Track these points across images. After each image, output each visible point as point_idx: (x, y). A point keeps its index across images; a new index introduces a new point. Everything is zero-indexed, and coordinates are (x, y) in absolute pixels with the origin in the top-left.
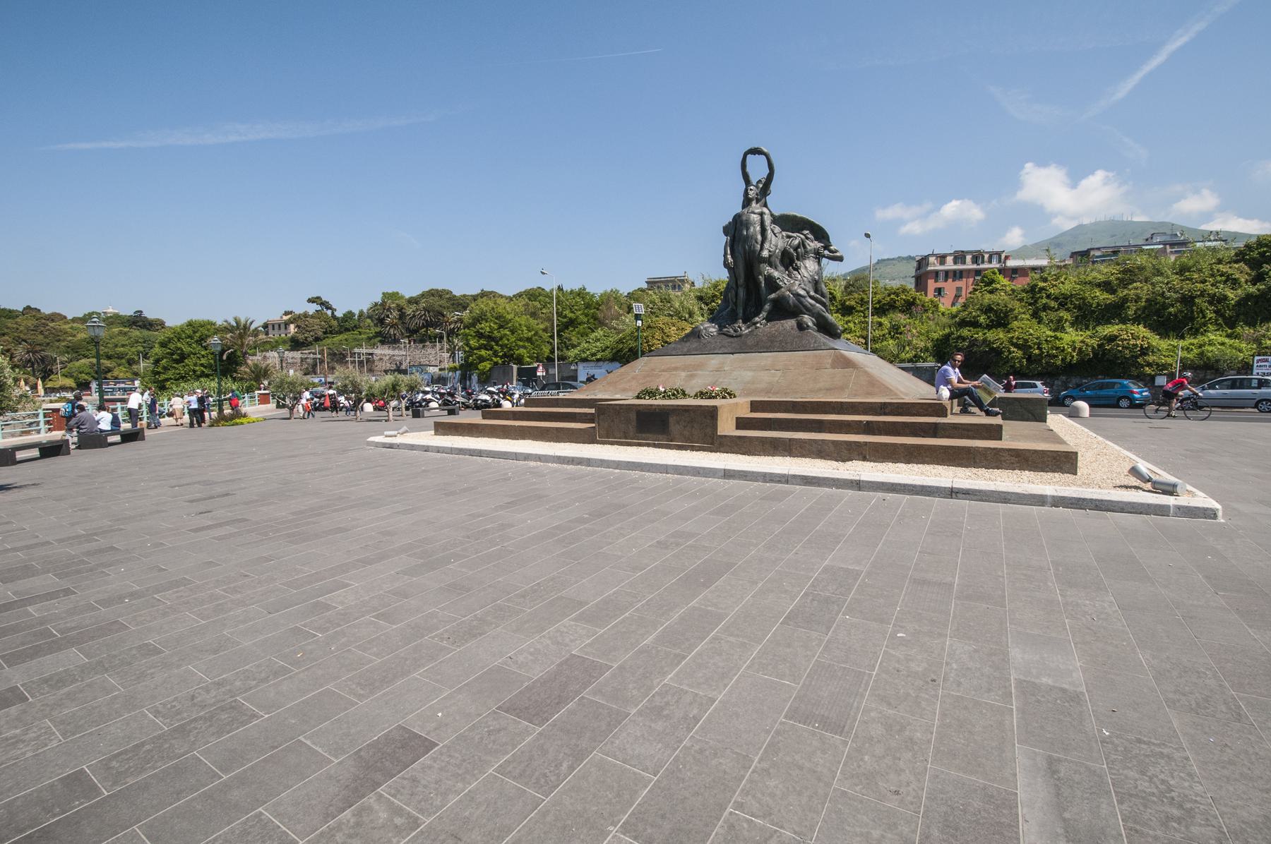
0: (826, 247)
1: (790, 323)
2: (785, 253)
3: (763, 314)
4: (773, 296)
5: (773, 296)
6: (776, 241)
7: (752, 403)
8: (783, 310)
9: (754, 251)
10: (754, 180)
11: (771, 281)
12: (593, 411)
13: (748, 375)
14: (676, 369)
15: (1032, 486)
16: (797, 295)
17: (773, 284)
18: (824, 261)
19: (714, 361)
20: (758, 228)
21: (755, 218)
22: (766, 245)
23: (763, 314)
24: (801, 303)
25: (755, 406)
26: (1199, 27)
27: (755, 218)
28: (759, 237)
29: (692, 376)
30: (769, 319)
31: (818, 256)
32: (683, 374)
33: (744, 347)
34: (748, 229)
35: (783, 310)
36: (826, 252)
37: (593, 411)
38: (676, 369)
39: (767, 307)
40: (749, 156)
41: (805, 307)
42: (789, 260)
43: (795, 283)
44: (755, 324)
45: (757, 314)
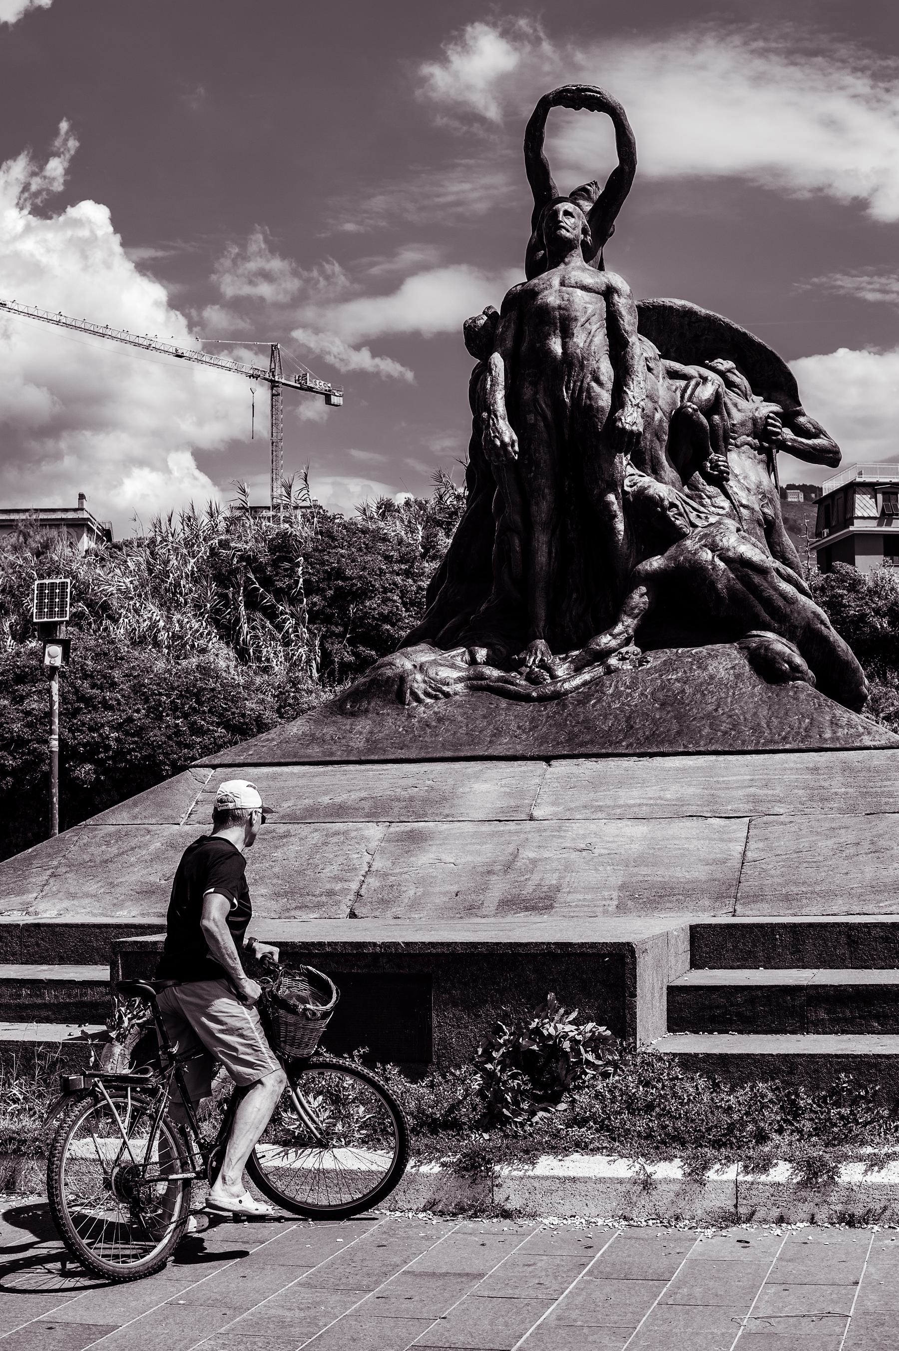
0: (790, 417)
1: (724, 661)
2: (680, 420)
3: (627, 624)
4: (656, 563)
5: (656, 563)
6: (653, 390)
7: (697, 933)
8: (704, 608)
9: (589, 411)
10: (564, 181)
11: (647, 513)
12: (101, 973)
13: (632, 836)
14: (339, 812)
15: (145, 1259)
16: (740, 564)
17: (654, 525)
18: (782, 459)
19: (485, 786)
20: (600, 340)
21: (586, 305)
22: (635, 392)
23: (627, 624)
24: (755, 590)
25: (706, 945)
26: (160, 254)
27: (586, 305)
28: (606, 370)
29: (414, 840)
30: (648, 637)
31: (766, 443)
32: (374, 832)
33: (577, 734)
34: (567, 335)
35: (704, 608)
36: (788, 434)
37: (101, 973)
38: (339, 812)
39: (639, 598)
40: (556, 113)
41: (767, 603)
42: (693, 443)
43: (728, 519)
44: (602, 656)
45: (607, 625)
